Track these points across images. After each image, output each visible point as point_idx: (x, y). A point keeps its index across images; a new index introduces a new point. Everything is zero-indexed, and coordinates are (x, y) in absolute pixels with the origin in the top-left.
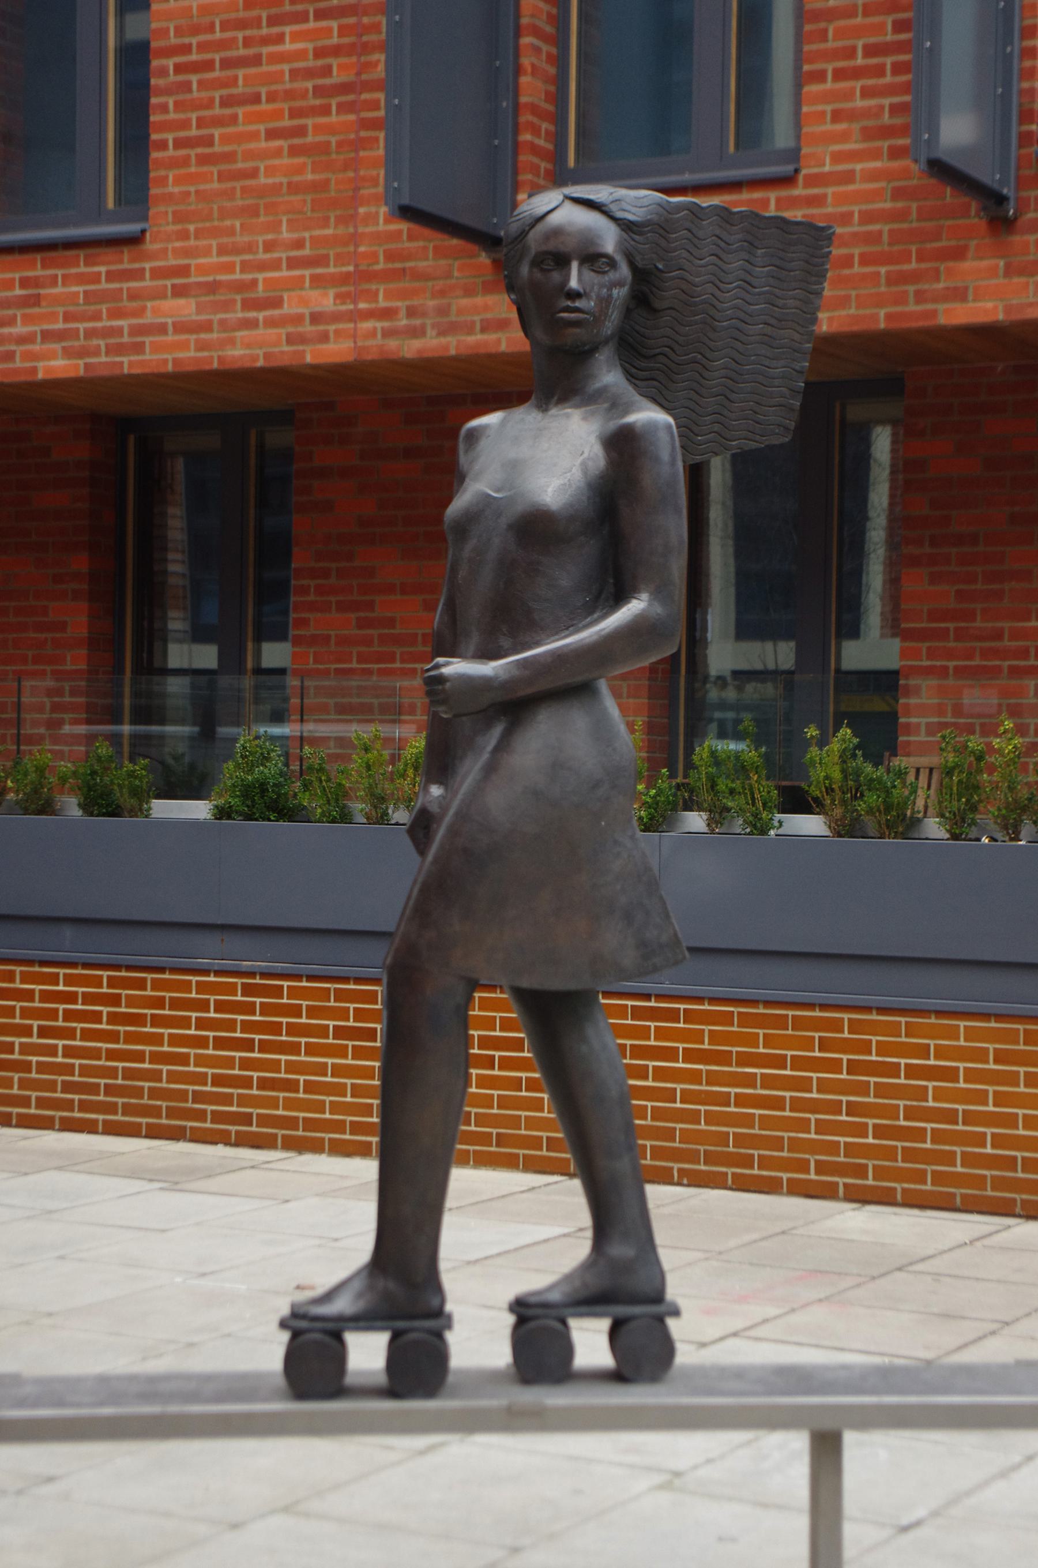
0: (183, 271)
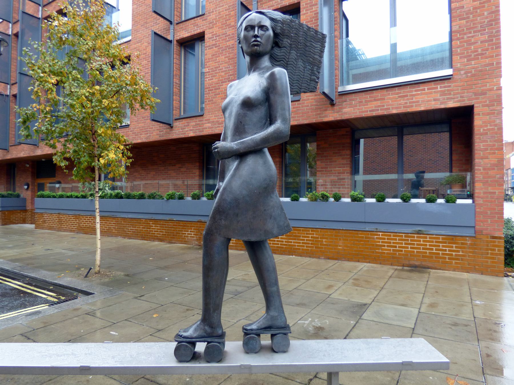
0: (209, 120)
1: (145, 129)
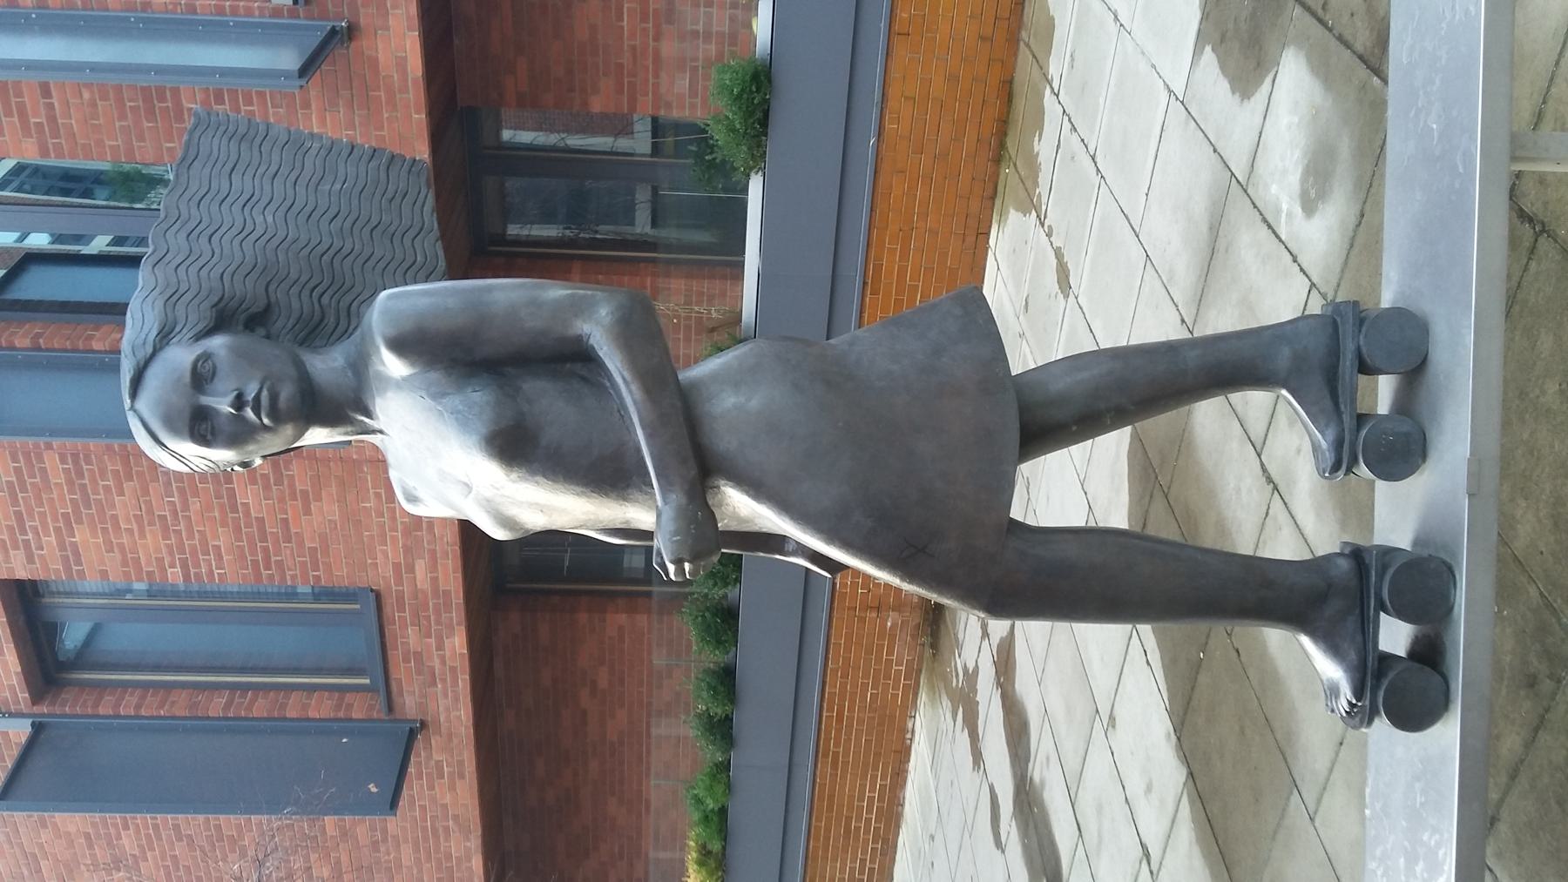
0: (397, 566)
1: (426, 839)
